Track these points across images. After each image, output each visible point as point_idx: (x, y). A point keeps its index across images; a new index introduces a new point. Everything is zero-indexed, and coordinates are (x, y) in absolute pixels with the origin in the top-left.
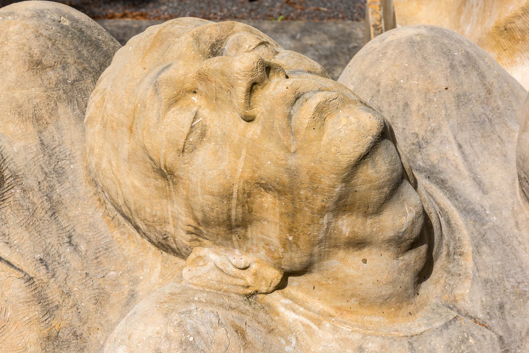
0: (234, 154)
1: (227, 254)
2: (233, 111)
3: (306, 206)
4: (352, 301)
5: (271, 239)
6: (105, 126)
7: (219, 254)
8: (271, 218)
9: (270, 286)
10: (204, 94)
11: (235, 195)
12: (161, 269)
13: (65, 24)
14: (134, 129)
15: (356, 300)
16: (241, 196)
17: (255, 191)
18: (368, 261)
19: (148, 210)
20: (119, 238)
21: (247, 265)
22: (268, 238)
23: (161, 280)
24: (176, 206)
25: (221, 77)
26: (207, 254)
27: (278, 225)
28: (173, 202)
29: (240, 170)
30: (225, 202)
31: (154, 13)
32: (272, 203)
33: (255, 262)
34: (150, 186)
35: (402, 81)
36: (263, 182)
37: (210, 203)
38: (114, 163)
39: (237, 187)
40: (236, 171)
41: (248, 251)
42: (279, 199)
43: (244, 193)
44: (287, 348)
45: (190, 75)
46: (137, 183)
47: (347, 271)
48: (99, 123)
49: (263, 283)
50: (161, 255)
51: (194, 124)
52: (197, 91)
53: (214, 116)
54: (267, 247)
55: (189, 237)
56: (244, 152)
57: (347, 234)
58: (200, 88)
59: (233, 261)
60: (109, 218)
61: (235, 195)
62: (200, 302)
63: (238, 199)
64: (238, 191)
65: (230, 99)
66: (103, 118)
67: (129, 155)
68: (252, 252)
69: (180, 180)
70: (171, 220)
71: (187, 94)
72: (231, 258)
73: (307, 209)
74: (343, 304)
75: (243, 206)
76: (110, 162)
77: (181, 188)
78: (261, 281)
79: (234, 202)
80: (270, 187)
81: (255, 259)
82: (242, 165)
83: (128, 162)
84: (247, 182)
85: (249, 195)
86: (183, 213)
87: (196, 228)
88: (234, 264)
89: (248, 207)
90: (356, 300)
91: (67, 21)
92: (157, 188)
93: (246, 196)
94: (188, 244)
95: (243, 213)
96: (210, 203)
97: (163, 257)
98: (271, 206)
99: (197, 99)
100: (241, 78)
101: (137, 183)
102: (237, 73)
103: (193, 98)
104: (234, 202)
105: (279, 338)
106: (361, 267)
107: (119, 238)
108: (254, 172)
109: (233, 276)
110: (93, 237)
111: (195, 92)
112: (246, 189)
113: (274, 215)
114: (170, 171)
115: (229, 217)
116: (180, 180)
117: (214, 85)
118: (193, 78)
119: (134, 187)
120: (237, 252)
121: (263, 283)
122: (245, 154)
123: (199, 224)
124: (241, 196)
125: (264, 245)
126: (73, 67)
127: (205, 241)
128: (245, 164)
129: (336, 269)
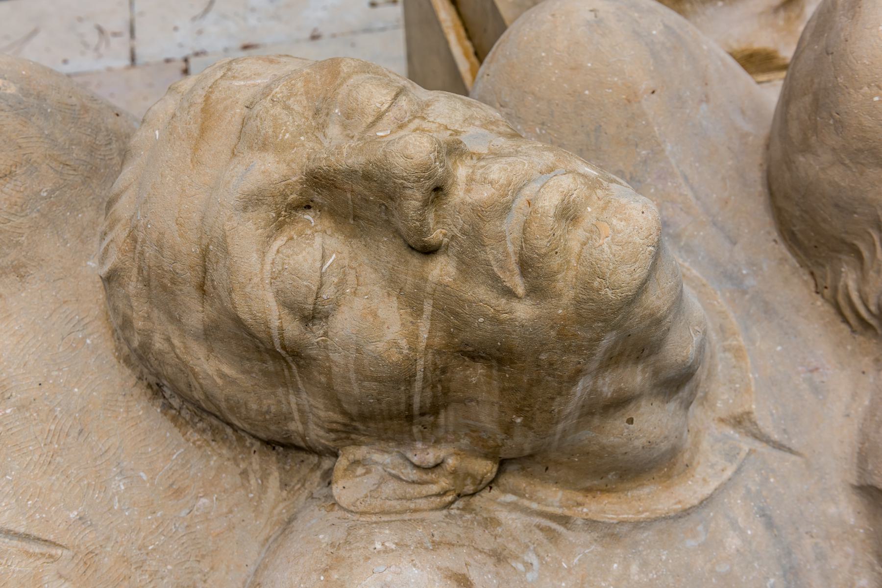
0: (409, 310)
1: (402, 450)
2: (395, 237)
3: (549, 375)
4: (610, 476)
5: (482, 424)
6: (147, 283)
7: (387, 452)
8: (483, 396)
9: (480, 483)
10: (326, 208)
11: (420, 375)
12: (280, 474)
13: (8, 91)
14: (208, 286)
15: (615, 475)
16: (429, 375)
17: (454, 362)
18: (635, 419)
19: (254, 407)
20: (198, 440)
21: (439, 461)
22: (478, 424)
23: (284, 493)
24: (304, 396)
25: (366, 183)
26: (368, 456)
27: (496, 408)
28: (297, 391)
29: (426, 336)
30: (403, 388)
31: (687, 456)
32: (486, 376)
33: (451, 455)
34: (252, 372)
35: (587, 92)
36: (470, 349)
37: (375, 393)
38: (176, 342)
39: (422, 363)
40: (417, 338)
41: (437, 442)
42: (499, 370)
43: (435, 370)
44: (530, 576)
45: (294, 179)
46: (226, 369)
47: (604, 441)
48: (135, 280)
49: (469, 481)
50: (274, 452)
51: (324, 270)
52: (311, 204)
53: (355, 247)
54: (474, 435)
55: (333, 436)
56: (428, 308)
57: (609, 395)
58: (318, 199)
59: (415, 460)
60: (174, 412)
61: (420, 375)
62: (386, 551)
63: (425, 378)
64: (425, 368)
65: (385, 217)
66: (140, 270)
67: (205, 330)
68: (446, 441)
69: (312, 362)
70: (296, 415)
71: (293, 212)
72: (409, 455)
73: (550, 379)
74: (595, 482)
75: (434, 387)
76: (168, 340)
77: (316, 374)
78: (465, 479)
79: (418, 385)
80: (484, 355)
81: (452, 450)
82: (428, 327)
83: (206, 339)
84: (439, 352)
85: (444, 371)
86: (321, 407)
87: (345, 425)
88: (418, 463)
89: (442, 386)
90: (615, 475)
91: (11, 84)
92: (265, 373)
93: (438, 372)
94: (331, 444)
95: (435, 396)
96: (375, 393)
97: (278, 454)
98: (482, 380)
99: (314, 217)
100: (410, 185)
101: (226, 369)
102: (403, 178)
103: (306, 217)
104: (418, 385)
105: (514, 565)
106: (626, 431)
107: (198, 440)
108: (451, 335)
109: (419, 483)
110: (119, 404)
111: (309, 207)
112: (439, 363)
113: (489, 392)
114: (293, 351)
115: (410, 406)
116: (312, 362)
117: (349, 195)
118: (302, 184)
119: (223, 376)
120: (419, 445)
121: (469, 481)
122: (431, 308)
123: (352, 420)
124: (429, 375)
125: (468, 432)
126: (44, 166)
127: (362, 438)
128: (432, 324)
129: (586, 442)
